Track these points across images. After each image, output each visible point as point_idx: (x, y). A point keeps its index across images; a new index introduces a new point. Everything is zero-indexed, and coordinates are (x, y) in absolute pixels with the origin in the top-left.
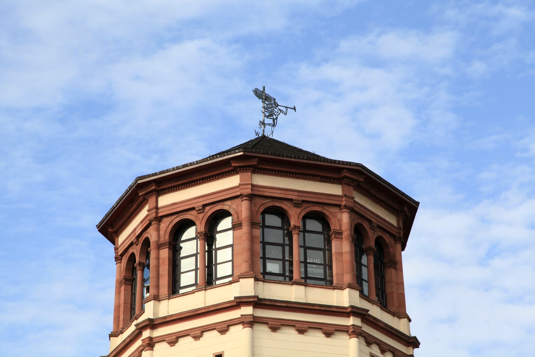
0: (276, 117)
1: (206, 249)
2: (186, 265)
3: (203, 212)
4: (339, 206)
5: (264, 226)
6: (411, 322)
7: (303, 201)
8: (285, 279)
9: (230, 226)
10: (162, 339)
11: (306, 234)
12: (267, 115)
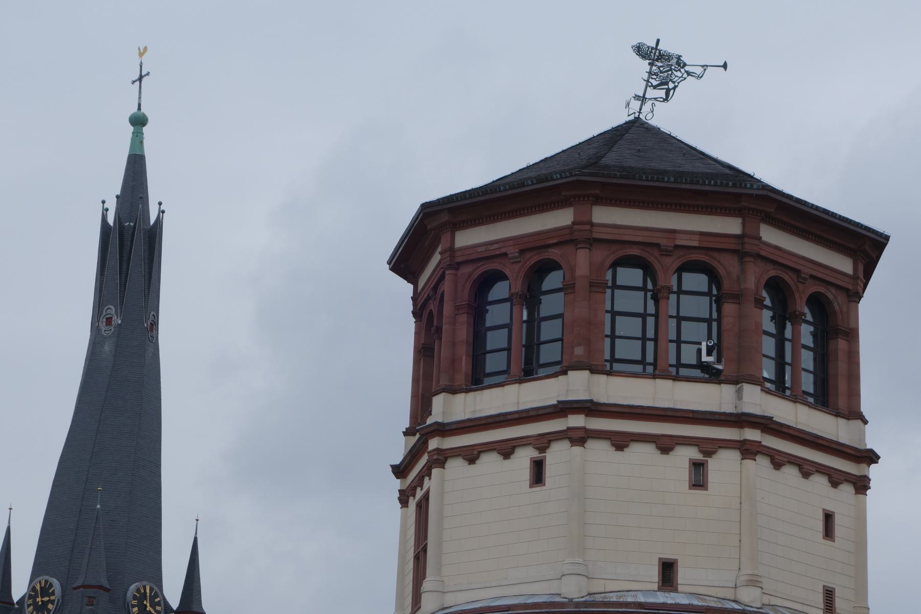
0: (675, 86)
1: (525, 318)
2: (496, 340)
3: (520, 262)
6: (867, 424)
8: (644, 369)
11: (682, 297)
12: (654, 84)
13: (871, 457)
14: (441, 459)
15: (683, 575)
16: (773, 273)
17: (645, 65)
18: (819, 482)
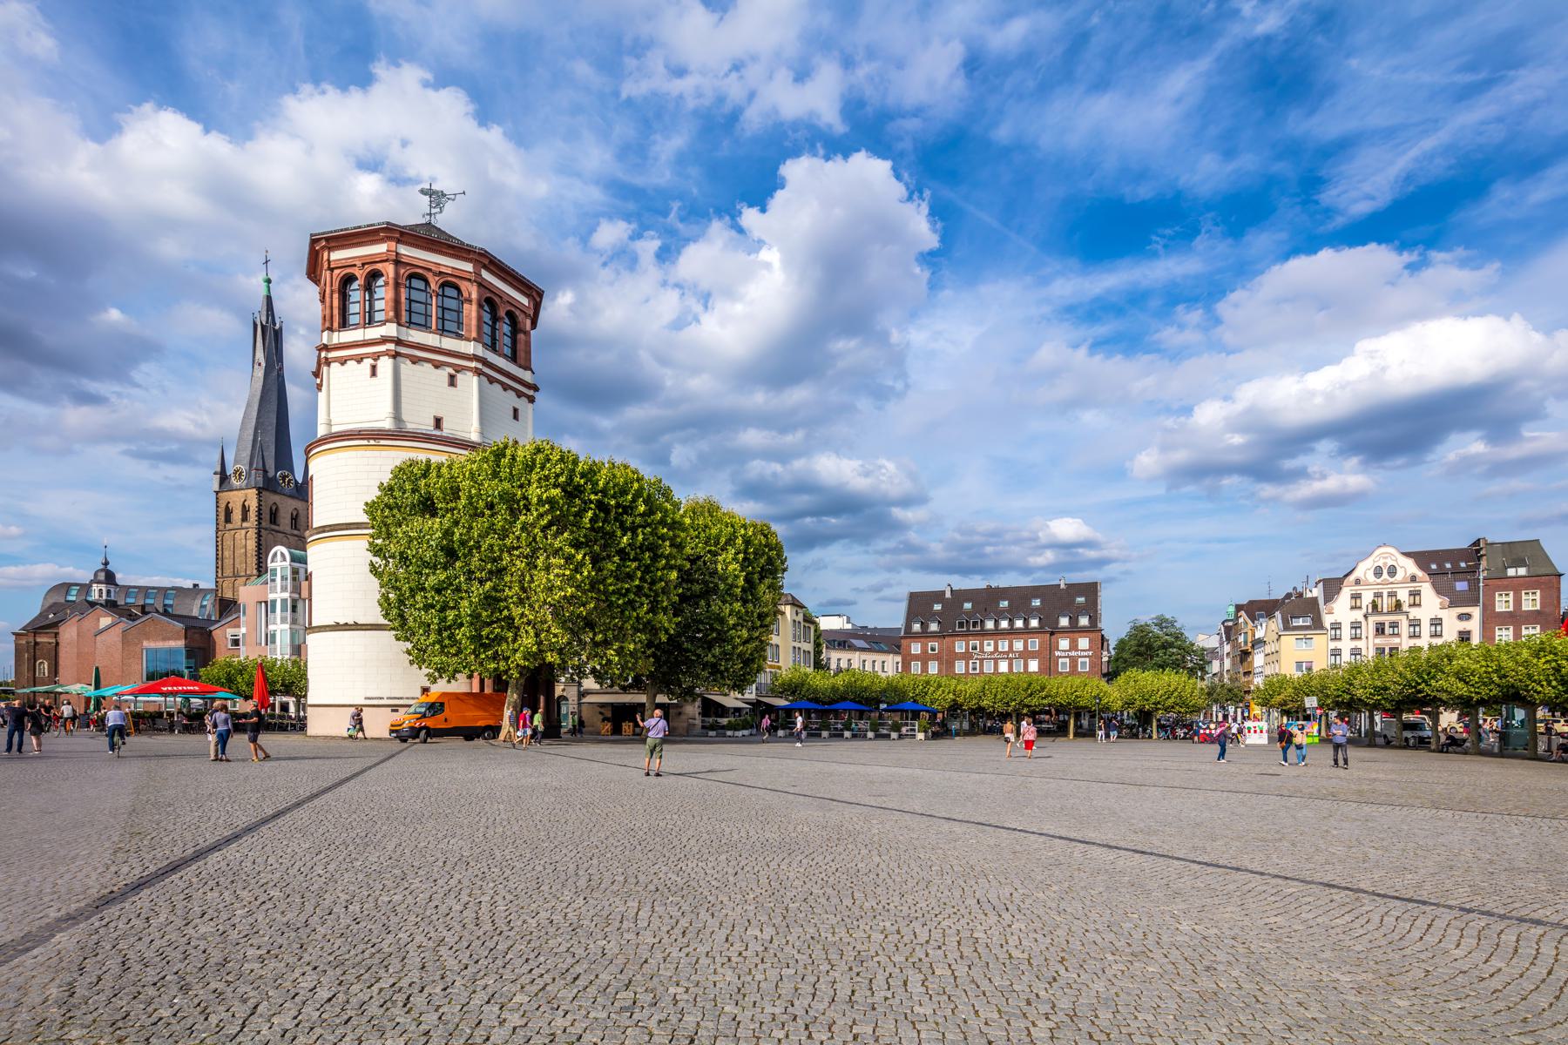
2: (379, 305)
4: (470, 280)
10: (336, 360)
14: (328, 362)
15: (445, 425)
16: (488, 295)
17: (427, 198)
18: (511, 394)
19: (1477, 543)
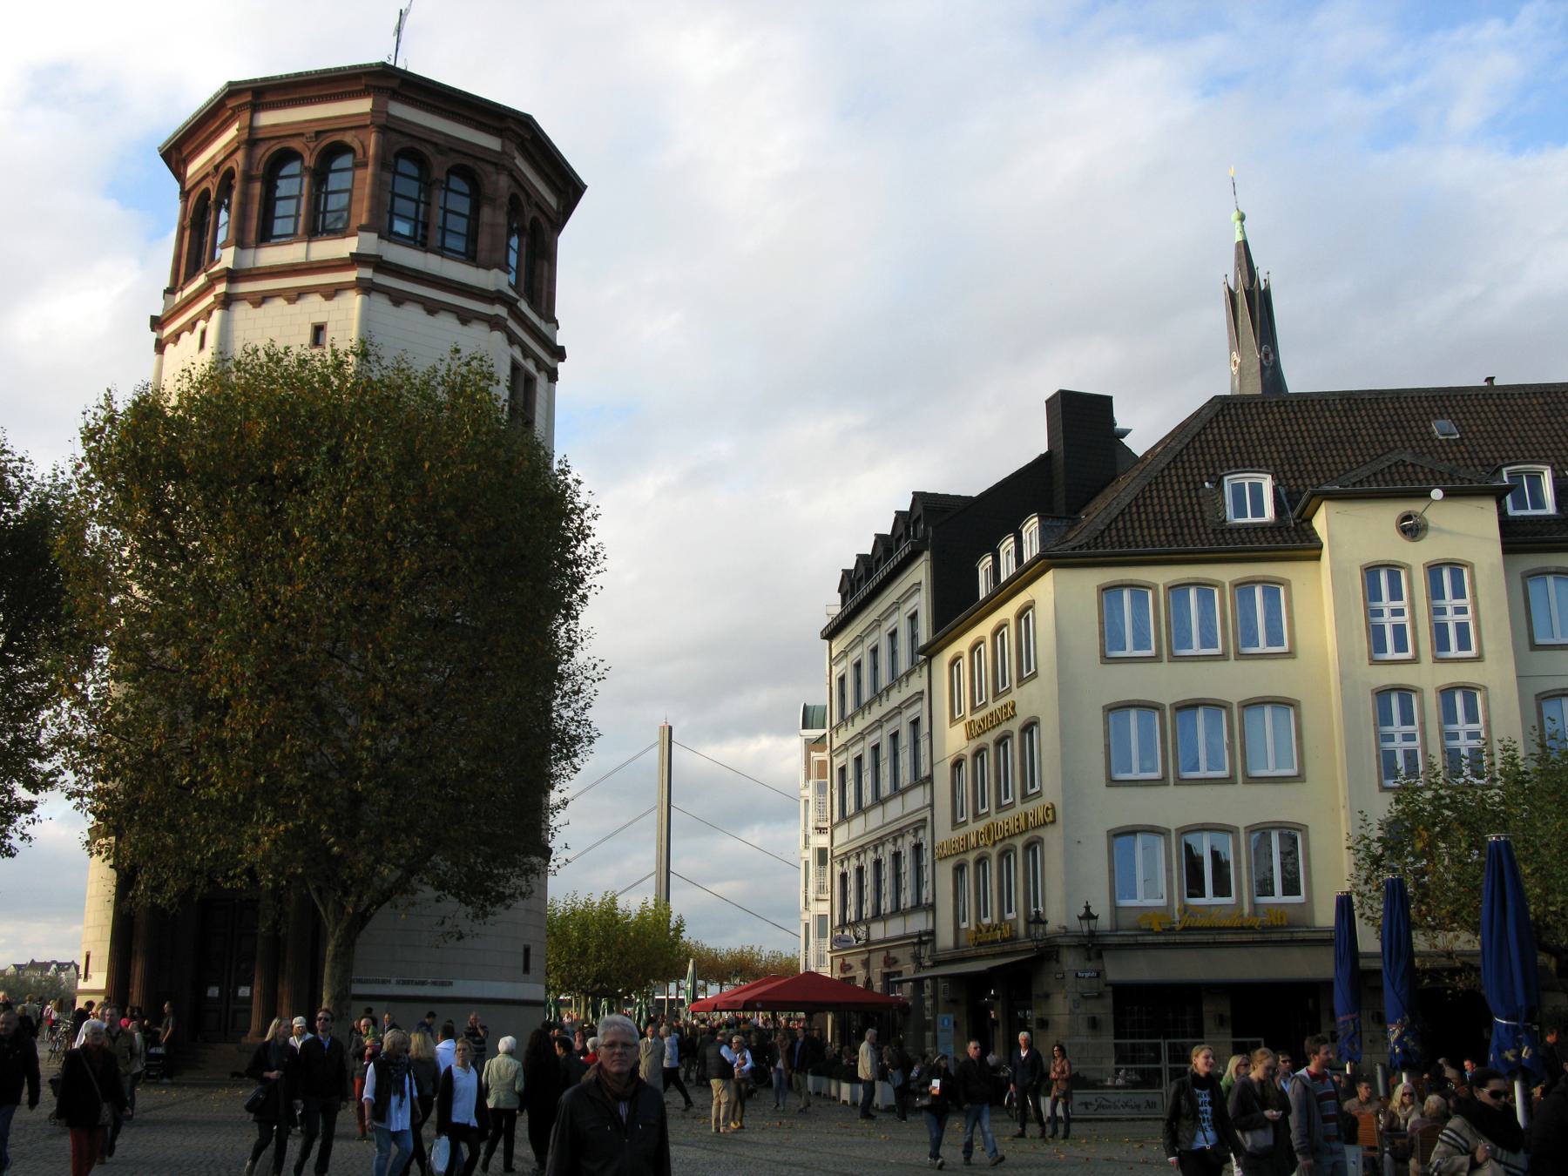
5: (396, 173)
7: (451, 149)
9: (350, 166)
13: (560, 354)
18: (447, 322)
19: (556, 322)
